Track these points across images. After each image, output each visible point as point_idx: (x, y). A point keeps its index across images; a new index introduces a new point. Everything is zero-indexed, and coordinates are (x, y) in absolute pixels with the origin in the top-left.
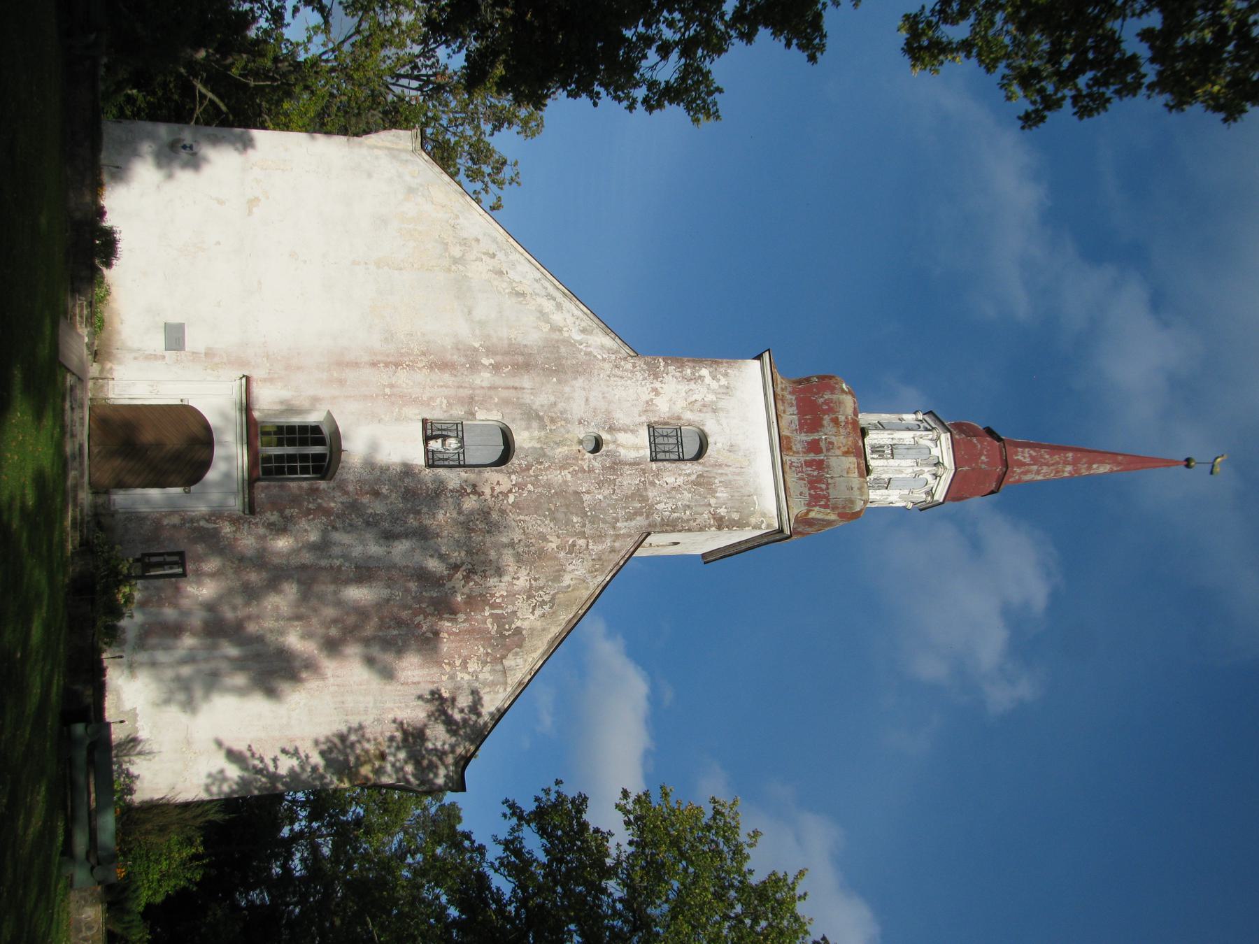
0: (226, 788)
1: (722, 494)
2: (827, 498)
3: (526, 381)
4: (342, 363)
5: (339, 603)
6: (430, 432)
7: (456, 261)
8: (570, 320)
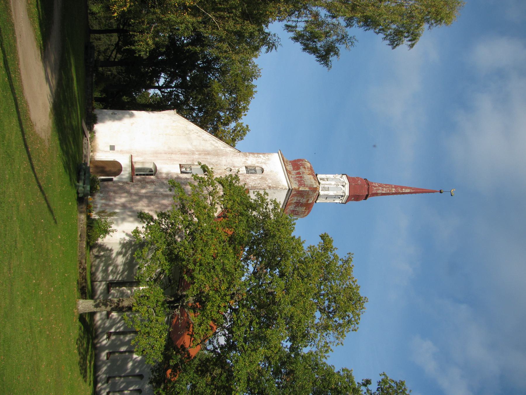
0: (125, 242)
1: (270, 181)
2: (304, 184)
3: (208, 157)
4: (156, 153)
5: (159, 203)
6: (181, 166)
7: (187, 134)
8: (220, 145)
